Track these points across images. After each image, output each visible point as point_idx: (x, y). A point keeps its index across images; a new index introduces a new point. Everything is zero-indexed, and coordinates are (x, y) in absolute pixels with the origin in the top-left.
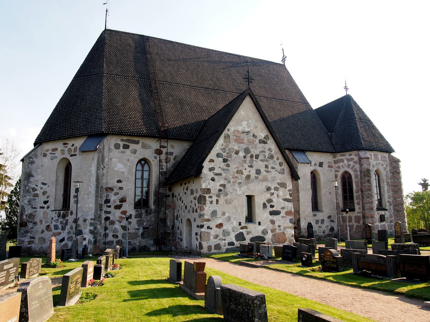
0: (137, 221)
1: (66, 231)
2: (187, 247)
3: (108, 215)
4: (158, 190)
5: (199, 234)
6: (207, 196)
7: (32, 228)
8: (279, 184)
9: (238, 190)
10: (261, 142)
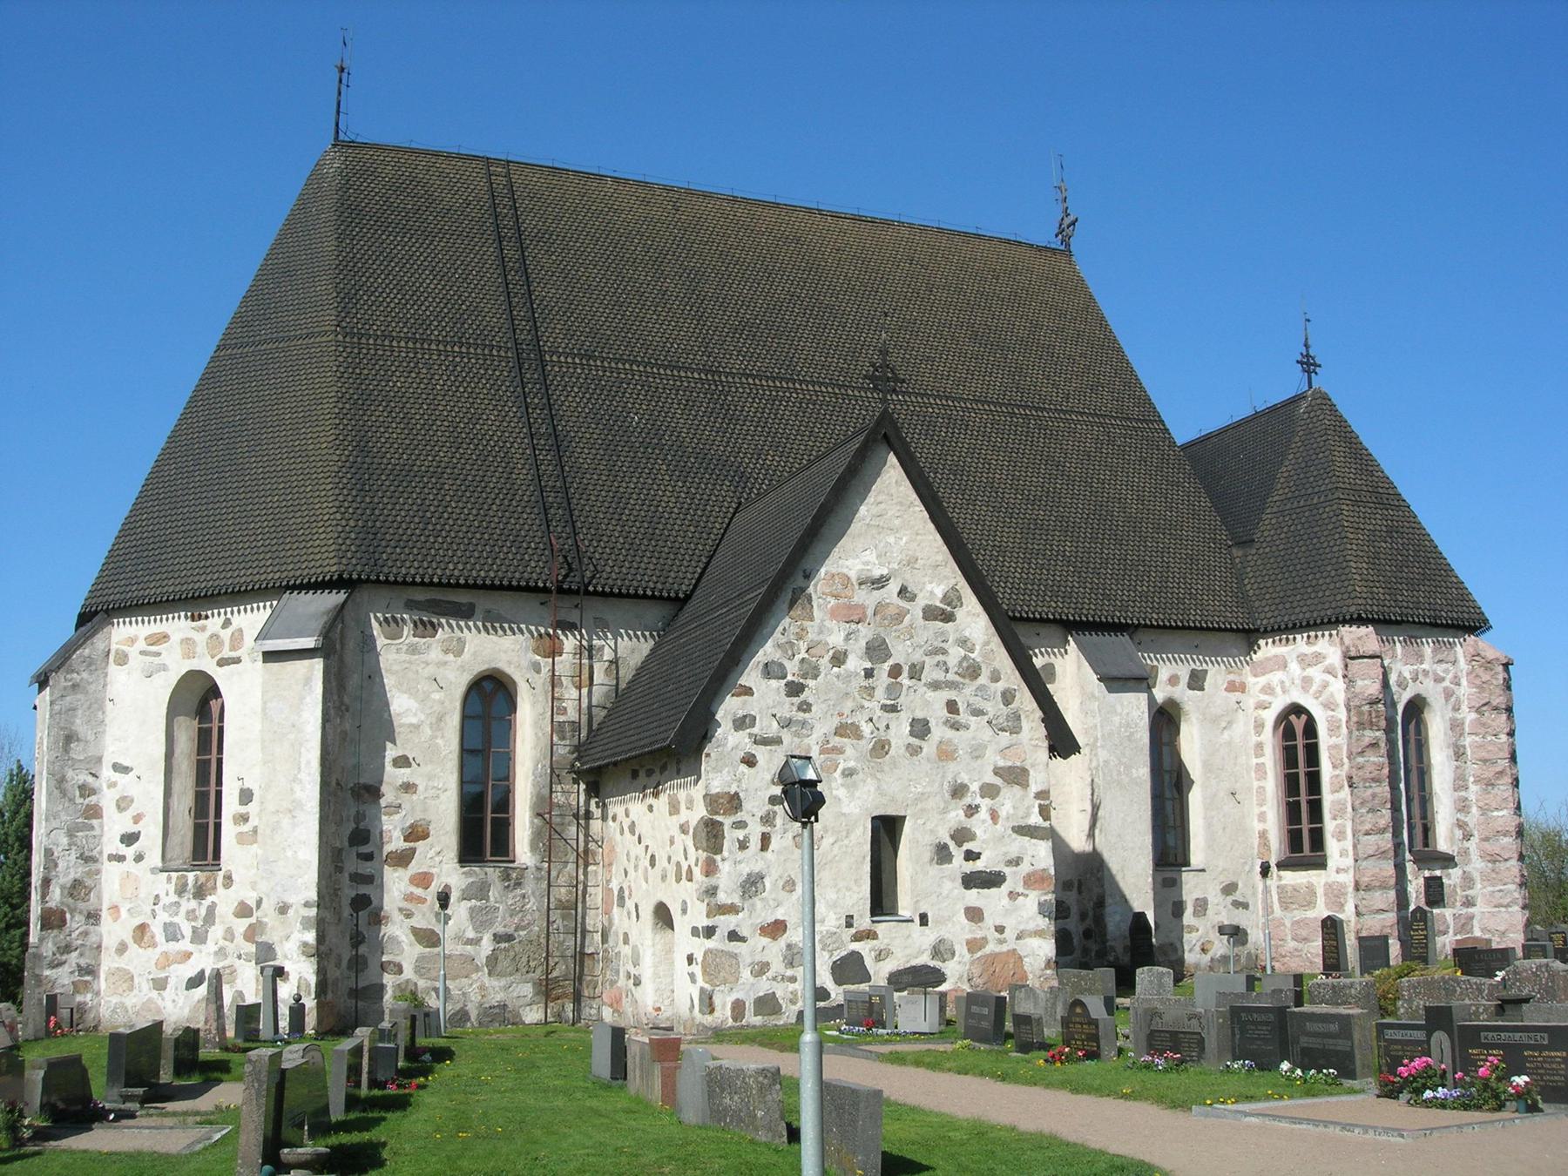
0: (472, 909)
1: (211, 946)
2: (659, 1009)
3: (364, 889)
4: (546, 791)
5: (700, 960)
6: (727, 821)
7: (86, 934)
8: (997, 772)
9: (845, 801)
10: (931, 614)
